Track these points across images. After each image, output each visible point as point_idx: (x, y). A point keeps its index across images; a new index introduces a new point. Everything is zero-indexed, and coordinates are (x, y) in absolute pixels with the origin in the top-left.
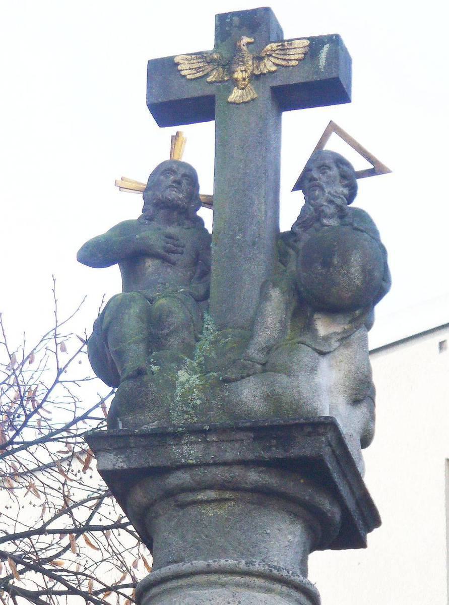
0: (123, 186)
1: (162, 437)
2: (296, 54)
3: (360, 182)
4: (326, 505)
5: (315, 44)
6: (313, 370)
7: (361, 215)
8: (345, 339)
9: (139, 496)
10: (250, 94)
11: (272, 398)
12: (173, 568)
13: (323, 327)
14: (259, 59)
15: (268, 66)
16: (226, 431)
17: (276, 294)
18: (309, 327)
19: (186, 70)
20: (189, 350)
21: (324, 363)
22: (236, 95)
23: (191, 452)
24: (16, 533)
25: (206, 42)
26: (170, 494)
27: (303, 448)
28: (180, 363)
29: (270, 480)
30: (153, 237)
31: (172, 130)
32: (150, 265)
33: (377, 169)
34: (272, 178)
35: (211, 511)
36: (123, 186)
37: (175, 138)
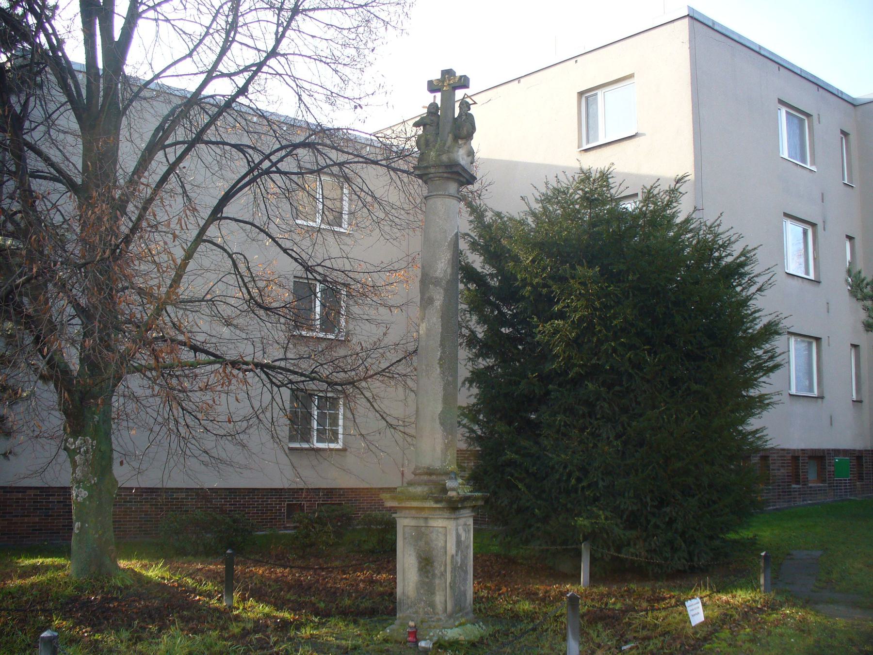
0: (424, 107)
1: (426, 168)
2: (457, 80)
3: (471, 106)
4: (462, 179)
5: (461, 77)
6: (458, 152)
7: (471, 115)
8: (465, 144)
9: (424, 178)
10: (448, 88)
11: (449, 158)
12: (430, 194)
13: (460, 142)
14: (449, 80)
15: (451, 82)
16: (439, 166)
17: (450, 135)
18: (457, 142)
19: (435, 83)
20: (434, 146)
21: (460, 150)
22: (445, 88)
23: (432, 170)
24: (115, 16)
25: (439, 77)
26: (430, 178)
27: (455, 169)
28: (431, 150)
29: (449, 176)
30: (428, 121)
31: (434, 94)
32: (428, 126)
33: (475, 103)
34: (183, 495)
35: (438, 182)
36: (424, 107)
37: (435, 96)
